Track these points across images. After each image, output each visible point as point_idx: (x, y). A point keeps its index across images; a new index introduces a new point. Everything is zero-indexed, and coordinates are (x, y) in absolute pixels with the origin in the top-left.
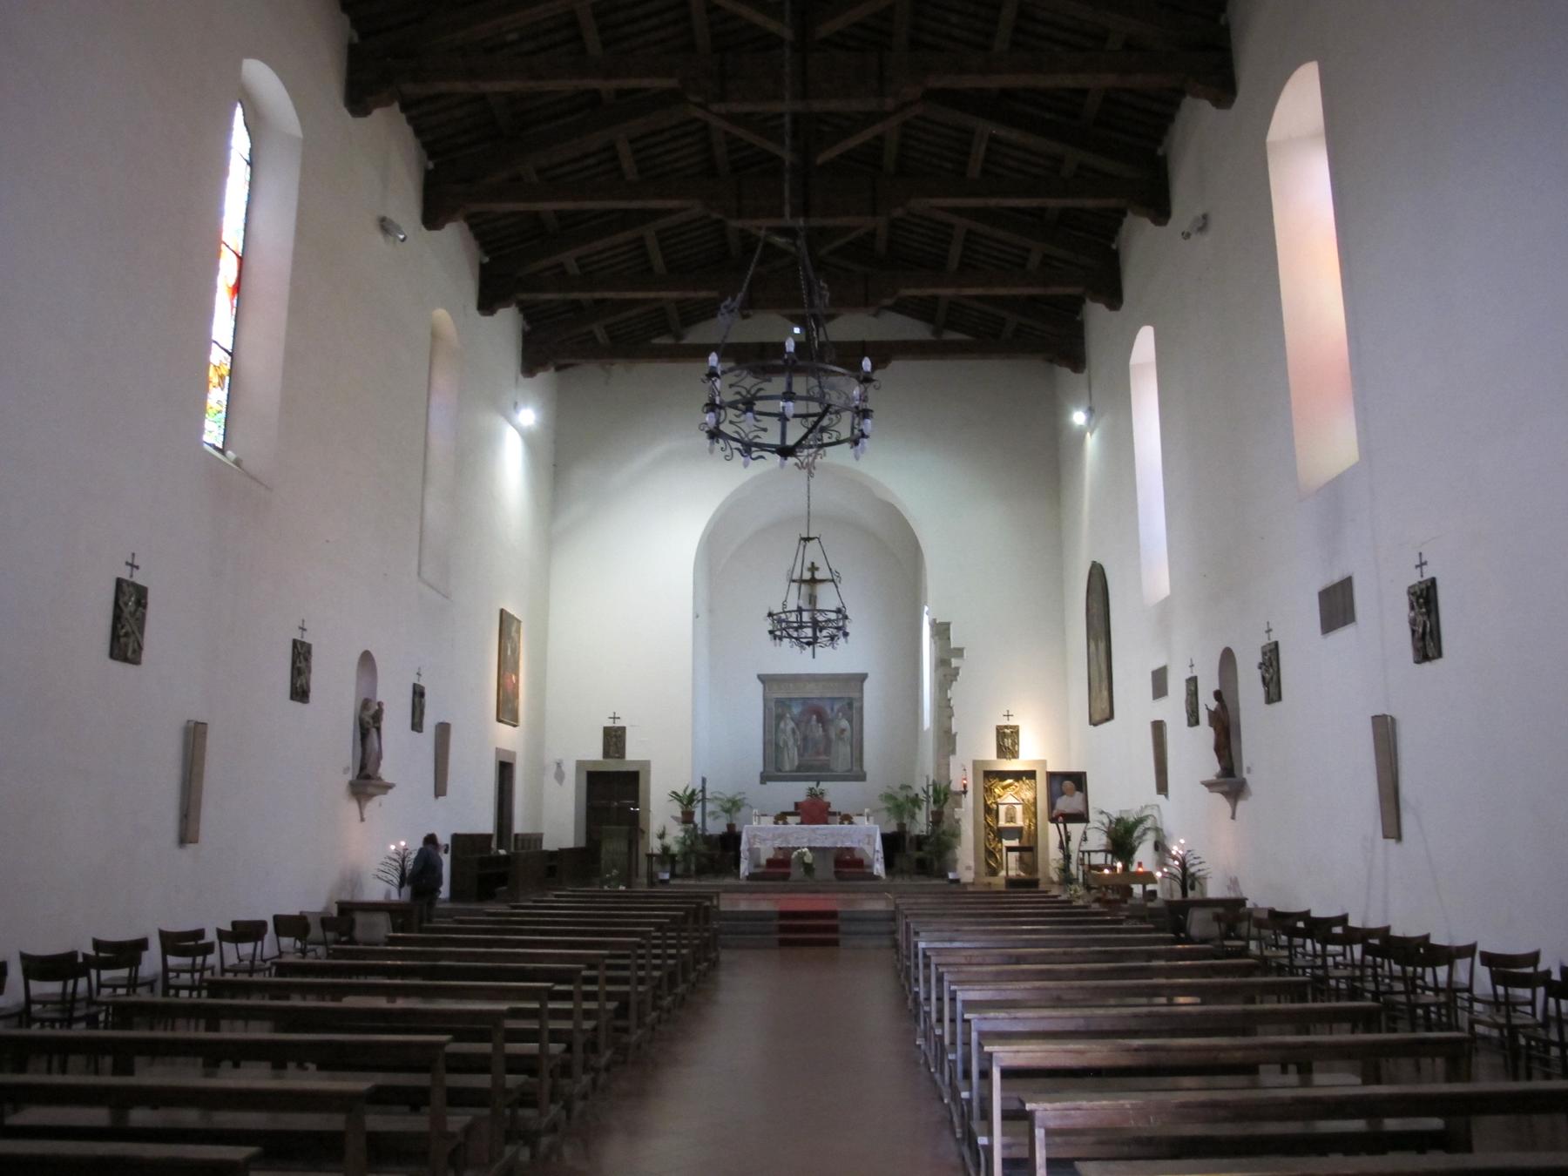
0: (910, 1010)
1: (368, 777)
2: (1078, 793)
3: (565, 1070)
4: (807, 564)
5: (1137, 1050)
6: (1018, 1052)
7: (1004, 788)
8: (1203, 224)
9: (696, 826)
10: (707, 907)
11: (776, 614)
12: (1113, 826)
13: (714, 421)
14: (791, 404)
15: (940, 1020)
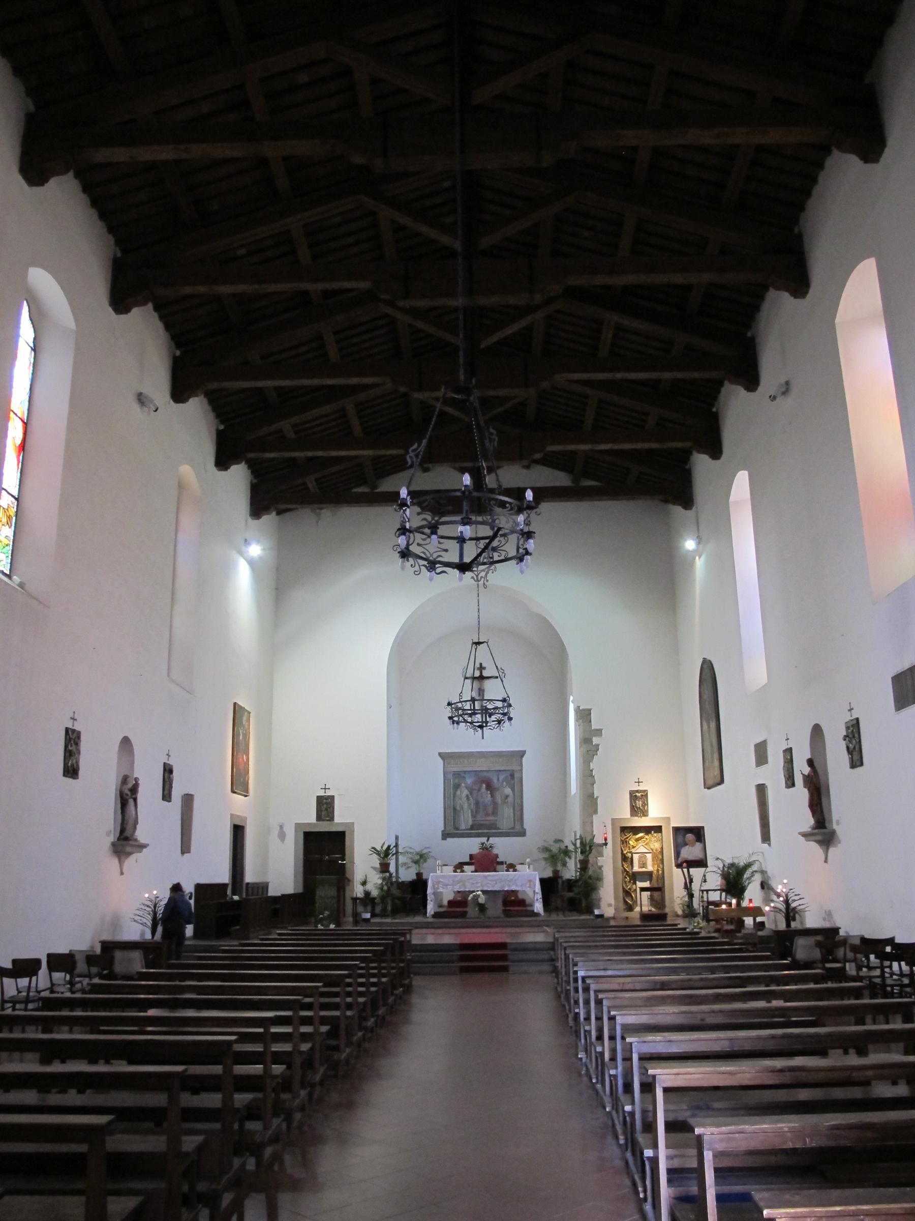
0: (571, 1027)
1: (127, 839)
2: (698, 844)
3: (285, 1084)
4: (477, 665)
5: (781, 1071)
6: (678, 1074)
7: (637, 840)
8: (786, 388)
9: (391, 874)
10: (402, 942)
11: (455, 703)
12: (726, 869)
13: (405, 542)
14: (468, 527)
15: (600, 1038)
